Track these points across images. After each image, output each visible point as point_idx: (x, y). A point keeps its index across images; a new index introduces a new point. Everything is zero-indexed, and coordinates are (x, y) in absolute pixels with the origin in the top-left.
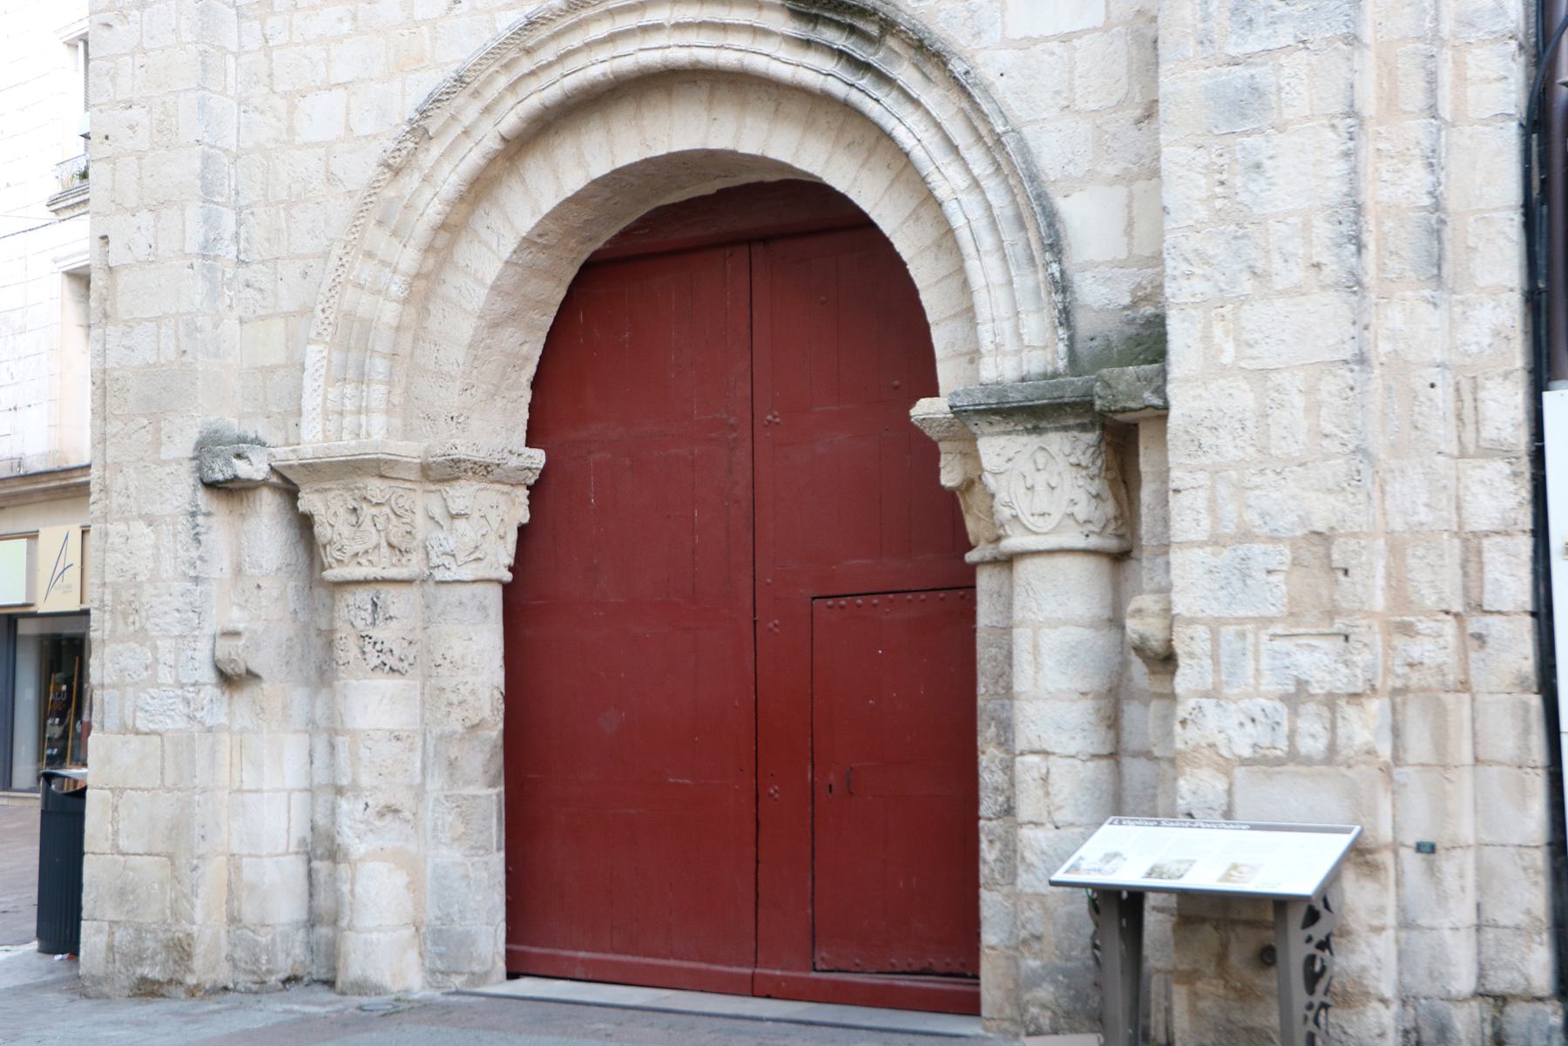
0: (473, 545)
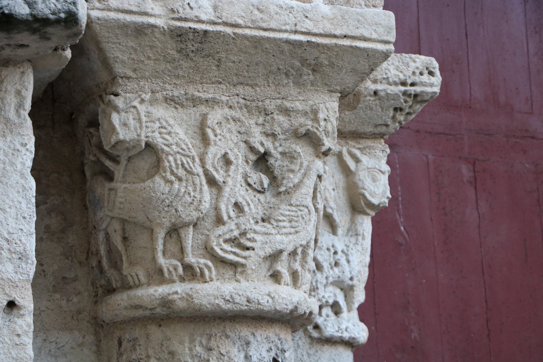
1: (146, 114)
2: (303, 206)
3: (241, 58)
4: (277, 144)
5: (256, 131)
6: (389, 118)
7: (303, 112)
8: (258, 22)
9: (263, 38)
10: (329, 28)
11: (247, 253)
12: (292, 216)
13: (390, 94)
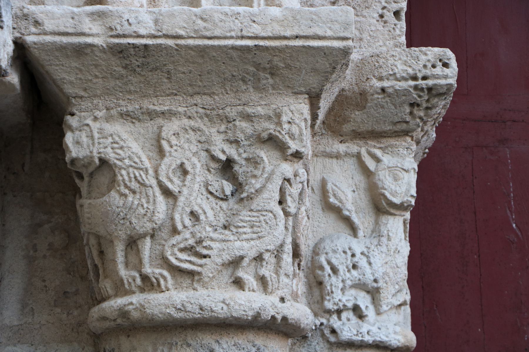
1: (99, 131)
2: (266, 211)
3: (190, 68)
4: (241, 151)
6: (405, 115)
7: (266, 117)
8: (202, 31)
9: (207, 47)
10: (279, 30)
11: (203, 261)
12: (253, 221)
13: (399, 90)
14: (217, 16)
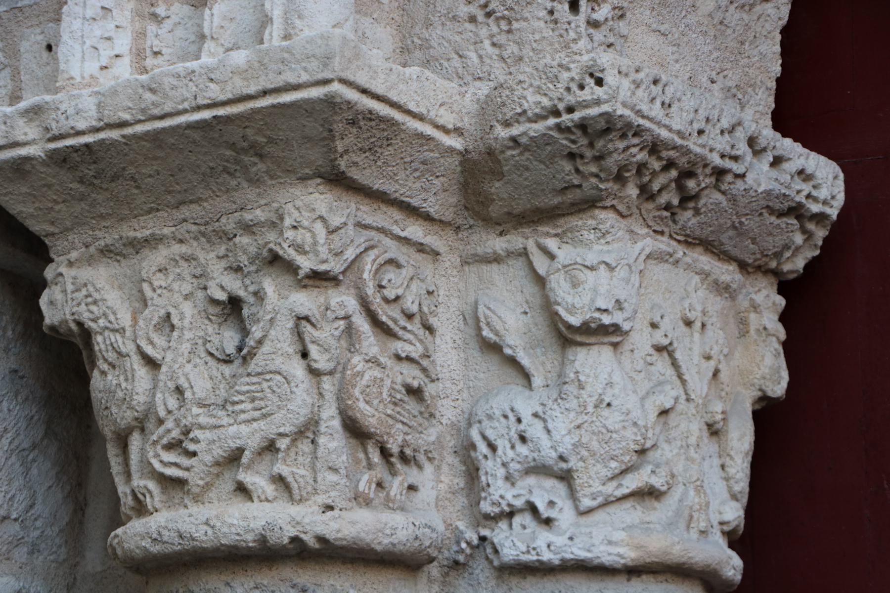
0: (631, 438)
2: (271, 372)
3: (155, 168)
5: (216, 268)
8: (149, 109)
13: (536, 137)
14: (168, 81)
